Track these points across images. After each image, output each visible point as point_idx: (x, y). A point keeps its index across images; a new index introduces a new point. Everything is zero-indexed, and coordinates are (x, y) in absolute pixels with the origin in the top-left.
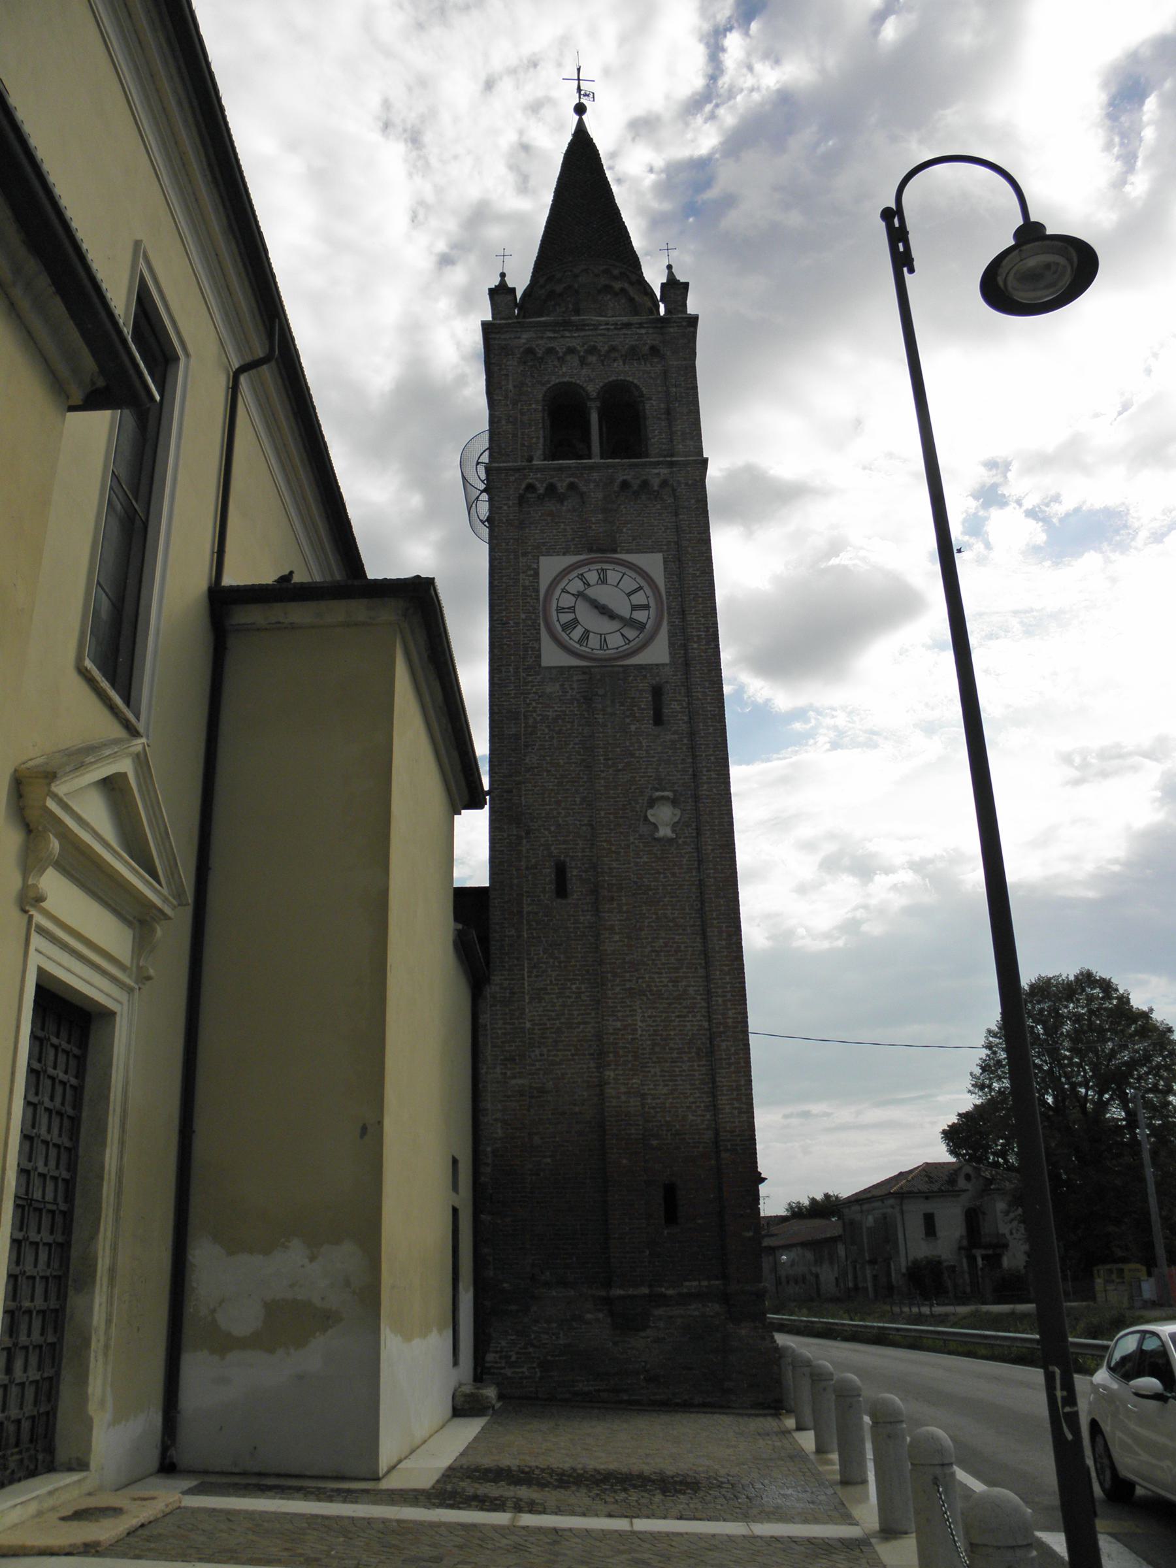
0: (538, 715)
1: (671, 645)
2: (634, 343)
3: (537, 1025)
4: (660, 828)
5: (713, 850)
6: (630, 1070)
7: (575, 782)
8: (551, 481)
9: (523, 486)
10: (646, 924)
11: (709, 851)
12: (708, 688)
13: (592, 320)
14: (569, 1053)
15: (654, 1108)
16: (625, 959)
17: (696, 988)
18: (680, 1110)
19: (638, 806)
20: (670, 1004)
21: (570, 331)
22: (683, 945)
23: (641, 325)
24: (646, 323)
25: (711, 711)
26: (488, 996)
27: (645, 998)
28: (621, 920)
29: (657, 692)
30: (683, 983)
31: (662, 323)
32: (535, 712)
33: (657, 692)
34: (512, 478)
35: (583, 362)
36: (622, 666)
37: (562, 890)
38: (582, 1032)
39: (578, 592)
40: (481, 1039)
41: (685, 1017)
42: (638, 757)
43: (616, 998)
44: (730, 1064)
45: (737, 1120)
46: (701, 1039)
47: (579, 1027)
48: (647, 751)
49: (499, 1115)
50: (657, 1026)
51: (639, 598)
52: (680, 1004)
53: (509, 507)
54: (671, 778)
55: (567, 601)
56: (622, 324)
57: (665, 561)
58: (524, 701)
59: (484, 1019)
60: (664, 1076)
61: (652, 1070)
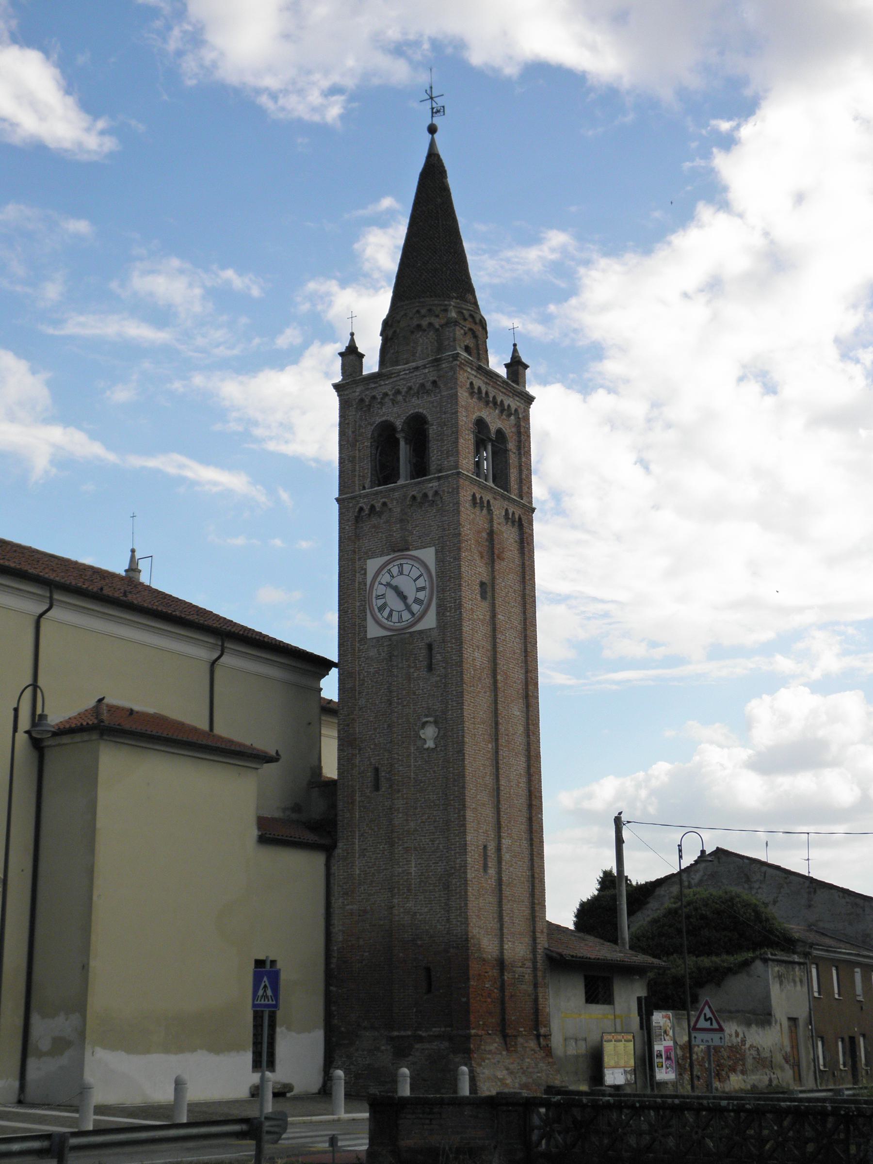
0: (366, 672)
1: (438, 614)
2: (421, 381)
3: (363, 871)
4: (428, 742)
5: (452, 754)
6: (405, 898)
7: (384, 715)
8: (372, 503)
9: (357, 510)
10: (419, 805)
11: (450, 756)
12: (454, 643)
13: (395, 370)
14: (378, 888)
15: (420, 921)
16: (403, 829)
17: (444, 845)
18: (434, 922)
19: (417, 728)
20: (430, 855)
21: (384, 380)
22: (437, 817)
23: (425, 367)
24: (428, 364)
25: (455, 660)
26: (336, 855)
27: (417, 852)
28: (403, 804)
29: (430, 647)
30: (437, 842)
31: (437, 362)
32: (364, 670)
33: (430, 647)
34: (351, 505)
35: (393, 401)
36: (410, 633)
37: (377, 787)
38: (385, 875)
39: (387, 582)
40: (332, 881)
41: (437, 863)
42: (417, 695)
43: (399, 854)
44: (456, 893)
45: (459, 929)
46: (444, 877)
47: (383, 872)
48: (422, 690)
49: (340, 928)
50: (423, 870)
51: (421, 583)
52: (435, 855)
53: (349, 527)
54: (435, 707)
55: (381, 590)
56: (413, 368)
57: (437, 552)
58: (358, 663)
59: (334, 869)
60: (426, 901)
61: (420, 897)
